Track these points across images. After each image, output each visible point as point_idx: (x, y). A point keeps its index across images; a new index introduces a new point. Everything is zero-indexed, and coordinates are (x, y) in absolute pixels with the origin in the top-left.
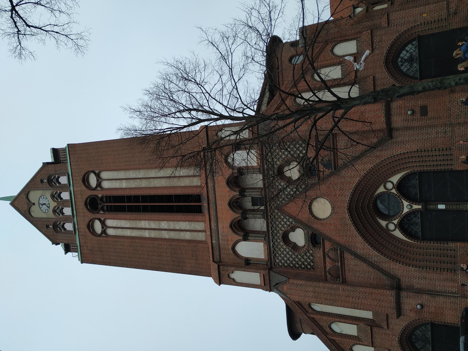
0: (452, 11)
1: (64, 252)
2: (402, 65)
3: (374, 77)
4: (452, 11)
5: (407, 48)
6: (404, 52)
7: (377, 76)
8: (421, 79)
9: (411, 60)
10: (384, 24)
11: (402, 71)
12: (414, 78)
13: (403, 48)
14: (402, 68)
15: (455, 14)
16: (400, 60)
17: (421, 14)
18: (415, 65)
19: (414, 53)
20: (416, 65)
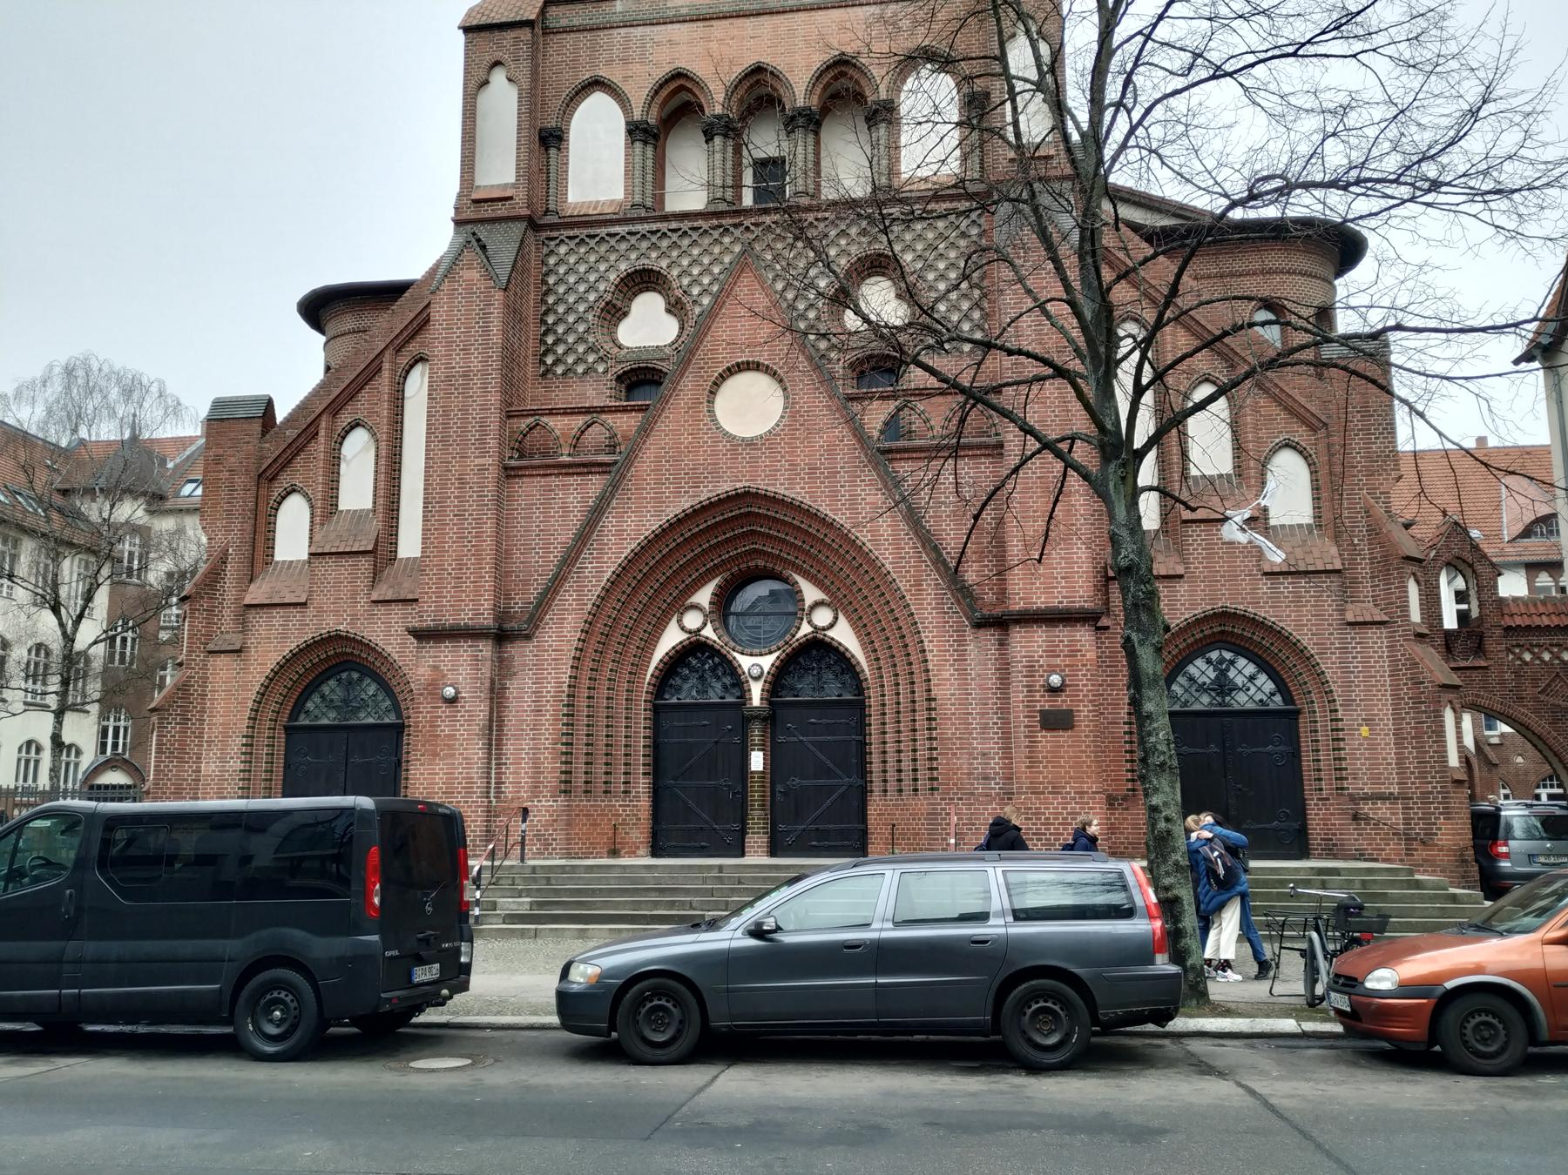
0: (1366, 808)
2: (1209, 662)
5: (1262, 678)
9: (1223, 686)
13: (1264, 666)
15: (1355, 817)
17: (1368, 721)
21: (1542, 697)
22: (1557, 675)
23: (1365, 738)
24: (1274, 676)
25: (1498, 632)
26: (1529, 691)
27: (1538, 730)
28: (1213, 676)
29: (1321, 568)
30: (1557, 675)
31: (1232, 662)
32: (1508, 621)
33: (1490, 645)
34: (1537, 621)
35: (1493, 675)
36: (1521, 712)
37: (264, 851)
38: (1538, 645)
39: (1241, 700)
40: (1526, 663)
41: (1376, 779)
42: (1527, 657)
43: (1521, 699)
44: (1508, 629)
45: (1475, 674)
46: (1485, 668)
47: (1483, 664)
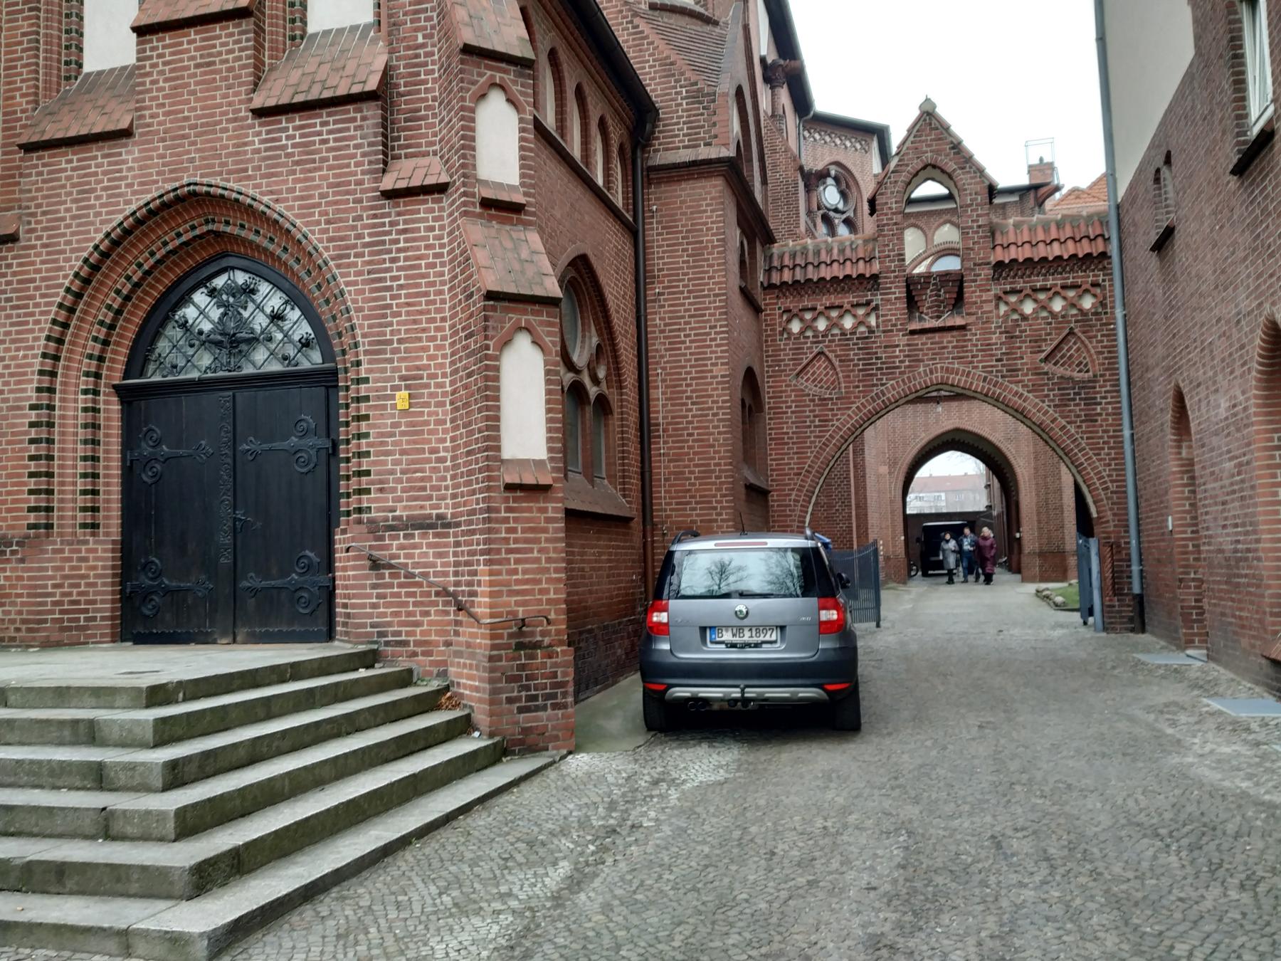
0: (394, 546)
1: (943, 111)
2: (212, 293)
3: (126, 133)
4: (394, 546)
5: (294, 314)
6: (275, 301)
7: (130, 153)
8: (126, 394)
9: (233, 341)
10: (404, 173)
11: (177, 296)
12: (140, 355)
13: (296, 297)
14: (200, 297)
15: (375, 565)
16: (241, 278)
17: (411, 381)
18: (206, 360)
19: (260, 355)
20: (203, 364)
21: (1046, 367)
22: (1071, 333)
23: (404, 412)
24: (310, 315)
25: (986, 272)
26: (1027, 359)
27: (1038, 417)
28: (216, 313)
29: (342, 91)
30: (1071, 333)
31: (249, 291)
32: (999, 255)
33: (971, 293)
34: (1042, 251)
35: (975, 336)
36: (1014, 390)
37: (316, 666)
38: (1044, 289)
39: (261, 360)
40: (1024, 318)
41: (417, 490)
42: (1028, 308)
43: (1013, 371)
44: (999, 265)
45: (947, 338)
46: (962, 328)
47: (959, 321)
